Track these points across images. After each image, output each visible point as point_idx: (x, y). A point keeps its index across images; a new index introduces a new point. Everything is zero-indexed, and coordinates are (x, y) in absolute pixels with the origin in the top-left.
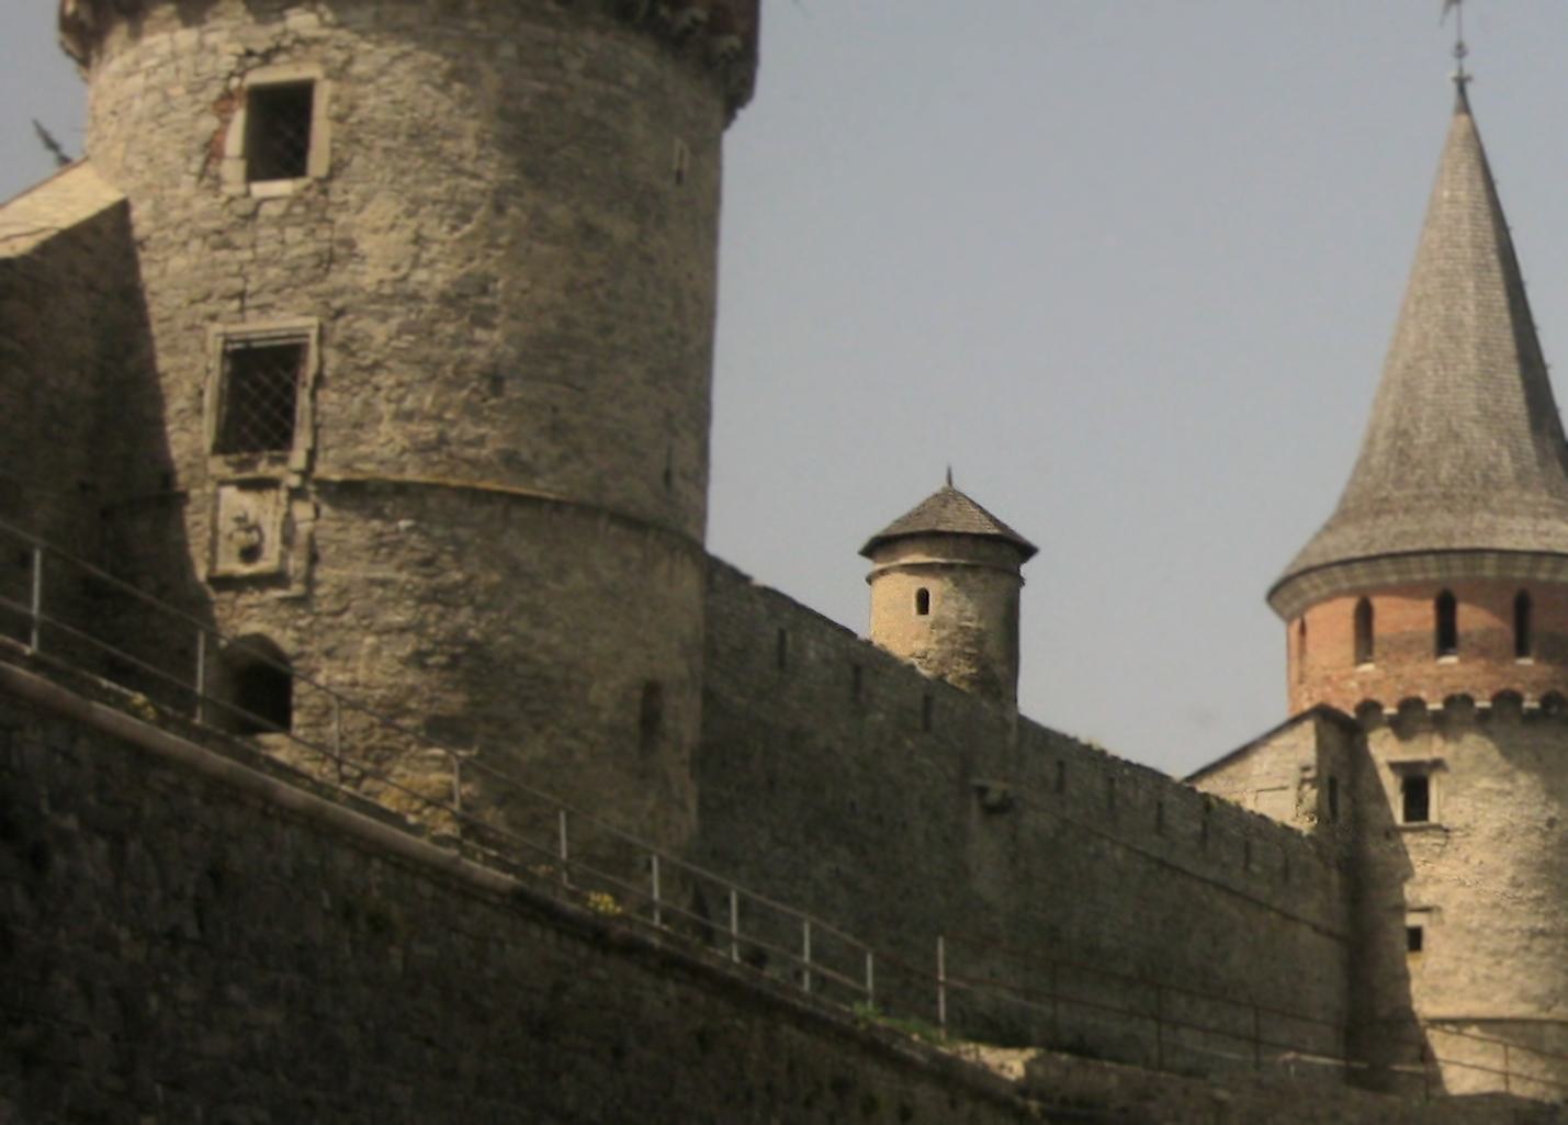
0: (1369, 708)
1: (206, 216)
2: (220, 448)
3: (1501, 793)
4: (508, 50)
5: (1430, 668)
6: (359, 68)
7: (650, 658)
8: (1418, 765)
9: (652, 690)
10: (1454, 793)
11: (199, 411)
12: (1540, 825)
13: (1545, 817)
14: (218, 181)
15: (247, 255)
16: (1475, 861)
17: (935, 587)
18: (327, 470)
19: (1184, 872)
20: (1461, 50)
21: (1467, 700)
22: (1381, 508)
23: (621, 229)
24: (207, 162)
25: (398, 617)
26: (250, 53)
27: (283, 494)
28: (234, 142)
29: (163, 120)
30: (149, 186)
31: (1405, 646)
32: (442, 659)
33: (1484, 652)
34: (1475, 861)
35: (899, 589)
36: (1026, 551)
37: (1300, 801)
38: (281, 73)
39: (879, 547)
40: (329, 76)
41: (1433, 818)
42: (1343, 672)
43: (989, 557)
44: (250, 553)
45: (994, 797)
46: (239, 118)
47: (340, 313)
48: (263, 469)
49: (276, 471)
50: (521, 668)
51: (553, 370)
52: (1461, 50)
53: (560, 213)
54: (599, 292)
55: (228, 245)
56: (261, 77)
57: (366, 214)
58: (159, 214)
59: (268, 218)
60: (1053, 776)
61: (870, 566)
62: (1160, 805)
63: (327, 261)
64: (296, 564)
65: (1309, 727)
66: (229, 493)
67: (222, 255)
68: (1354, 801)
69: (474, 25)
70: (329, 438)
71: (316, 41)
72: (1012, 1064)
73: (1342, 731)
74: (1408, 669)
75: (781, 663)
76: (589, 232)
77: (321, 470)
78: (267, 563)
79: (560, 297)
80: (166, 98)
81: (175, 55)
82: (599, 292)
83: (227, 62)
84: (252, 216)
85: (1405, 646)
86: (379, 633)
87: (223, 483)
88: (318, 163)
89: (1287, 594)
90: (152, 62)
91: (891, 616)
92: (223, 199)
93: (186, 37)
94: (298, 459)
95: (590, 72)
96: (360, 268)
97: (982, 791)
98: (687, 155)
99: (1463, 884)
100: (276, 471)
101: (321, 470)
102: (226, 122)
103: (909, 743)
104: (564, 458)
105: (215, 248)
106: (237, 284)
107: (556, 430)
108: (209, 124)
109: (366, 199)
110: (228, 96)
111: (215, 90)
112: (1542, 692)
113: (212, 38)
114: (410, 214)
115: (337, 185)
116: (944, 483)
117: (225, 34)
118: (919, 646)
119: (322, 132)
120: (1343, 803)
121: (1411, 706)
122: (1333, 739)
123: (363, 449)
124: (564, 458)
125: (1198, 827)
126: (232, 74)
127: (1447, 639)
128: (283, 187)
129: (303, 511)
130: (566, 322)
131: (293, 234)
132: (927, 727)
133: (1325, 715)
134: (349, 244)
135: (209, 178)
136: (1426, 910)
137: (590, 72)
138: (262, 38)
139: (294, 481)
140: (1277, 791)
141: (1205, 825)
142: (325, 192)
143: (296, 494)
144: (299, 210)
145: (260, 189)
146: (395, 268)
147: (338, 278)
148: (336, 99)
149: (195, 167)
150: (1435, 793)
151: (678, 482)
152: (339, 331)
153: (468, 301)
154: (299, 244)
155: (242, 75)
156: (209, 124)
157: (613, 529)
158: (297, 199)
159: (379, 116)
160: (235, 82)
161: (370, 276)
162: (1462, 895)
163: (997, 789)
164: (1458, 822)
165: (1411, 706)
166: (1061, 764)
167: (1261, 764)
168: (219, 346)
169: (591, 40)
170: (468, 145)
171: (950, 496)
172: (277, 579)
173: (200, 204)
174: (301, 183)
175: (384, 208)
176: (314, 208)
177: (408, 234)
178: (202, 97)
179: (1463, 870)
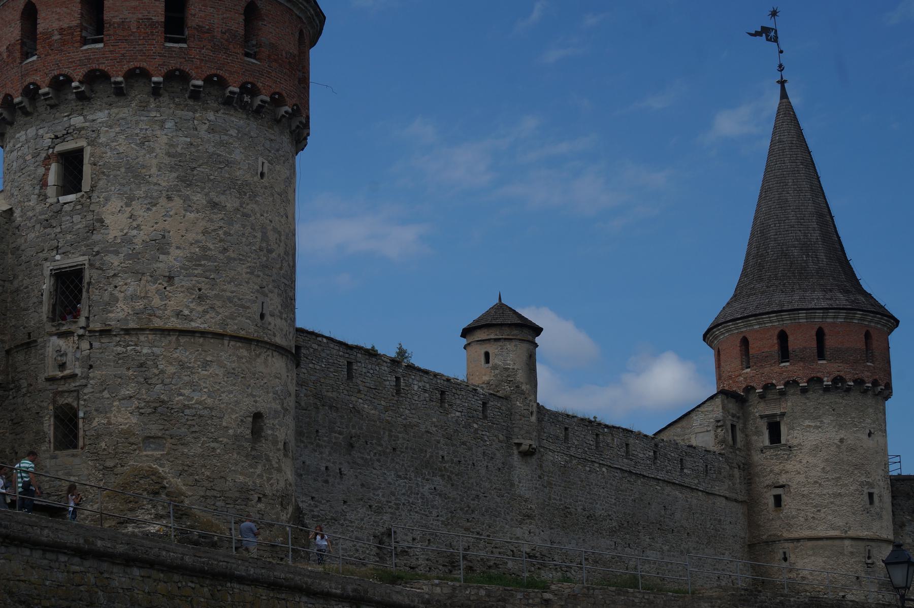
0: (749, 389)
1: (41, 214)
3: (817, 427)
4: (169, 124)
5: (776, 369)
6: (103, 139)
7: (256, 402)
8: (774, 415)
9: (258, 416)
10: (793, 429)
11: (41, 302)
12: (836, 441)
13: (838, 438)
14: (46, 197)
15: (58, 230)
16: (804, 461)
17: (492, 349)
18: (96, 326)
19: (644, 476)
20: (781, 68)
23: (230, 202)
24: (41, 188)
26: (56, 137)
27: (76, 338)
28: (52, 178)
29: (24, 171)
30: (20, 202)
32: (150, 410)
34: (804, 461)
36: (538, 330)
37: (716, 437)
38: (70, 145)
40: (89, 144)
41: (783, 442)
42: (737, 373)
44: (62, 366)
45: (525, 447)
46: (54, 167)
47: (98, 253)
49: (73, 328)
50: (187, 412)
51: (199, 271)
52: (781, 68)
53: (199, 198)
54: (221, 232)
55: (51, 226)
56: (59, 148)
57: (107, 206)
58: (23, 214)
59: (66, 212)
60: (562, 436)
61: (464, 341)
62: (627, 445)
63: (92, 230)
65: (718, 401)
66: (54, 338)
67: (48, 230)
68: (747, 435)
69: (153, 114)
71: (83, 128)
74: (767, 370)
75: (398, 392)
76: (214, 205)
77: (92, 326)
79: (200, 237)
80: (25, 161)
81: (27, 141)
82: (221, 232)
83: (47, 142)
84: (59, 212)
86: (120, 400)
87: (51, 335)
88: (86, 186)
90: (19, 145)
92: (48, 205)
94: (82, 321)
95: (211, 130)
96: (106, 231)
97: (519, 445)
98: (266, 164)
99: (799, 473)
100: (73, 328)
101: (92, 326)
102: (48, 169)
103: (475, 426)
104: (205, 312)
105: (45, 228)
106: (55, 243)
107: (201, 298)
108: (41, 171)
109: (107, 199)
110: (48, 157)
111: (43, 155)
112: (832, 377)
113: (41, 132)
114: (127, 205)
115: (95, 195)
116: (497, 301)
117: (46, 129)
118: (486, 378)
119: (87, 169)
120: (740, 436)
121: (768, 387)
122: (732, 406)
123: (111, 315)
124: (205, 312)
125: (652, 454)
126: (49, 147)
128: (71, 197)
129: (85, 345)
130: (204, 249)
131: (77, 218)
132: (485, 417)
134: (101, 221)
135: (43, 197)
136: (783, 486)
137: (211, 130)
138: (60, 130)
139: (81, 332)
141: (655, 452)
142: (90, 198)
144: (79, 207)
145: (63, 199)
146: (122, 230)
147: (96, 237)
148: (92, 155)
149: (37, 191)
150: (784, 429)
151: (268, 318)
154: (79, 222)
155: (53, 148)
156: (41, 171)
157: (232, 343)
158: (78, 202)
159: (112, 161)
160: (51, 151)
162: (801, 478)
163: (526, 444)
164: (795, 442)
165: (768, 387)
166: (566, 429)
167: (697, 420)
168: (49, 272)
169: (211, 116)
171: (501, 307)
173: (39, 208)
174: (79, 194)
176: (84, 207)
177: (127, 215)
178: (38, 159)
179: (798, 466)
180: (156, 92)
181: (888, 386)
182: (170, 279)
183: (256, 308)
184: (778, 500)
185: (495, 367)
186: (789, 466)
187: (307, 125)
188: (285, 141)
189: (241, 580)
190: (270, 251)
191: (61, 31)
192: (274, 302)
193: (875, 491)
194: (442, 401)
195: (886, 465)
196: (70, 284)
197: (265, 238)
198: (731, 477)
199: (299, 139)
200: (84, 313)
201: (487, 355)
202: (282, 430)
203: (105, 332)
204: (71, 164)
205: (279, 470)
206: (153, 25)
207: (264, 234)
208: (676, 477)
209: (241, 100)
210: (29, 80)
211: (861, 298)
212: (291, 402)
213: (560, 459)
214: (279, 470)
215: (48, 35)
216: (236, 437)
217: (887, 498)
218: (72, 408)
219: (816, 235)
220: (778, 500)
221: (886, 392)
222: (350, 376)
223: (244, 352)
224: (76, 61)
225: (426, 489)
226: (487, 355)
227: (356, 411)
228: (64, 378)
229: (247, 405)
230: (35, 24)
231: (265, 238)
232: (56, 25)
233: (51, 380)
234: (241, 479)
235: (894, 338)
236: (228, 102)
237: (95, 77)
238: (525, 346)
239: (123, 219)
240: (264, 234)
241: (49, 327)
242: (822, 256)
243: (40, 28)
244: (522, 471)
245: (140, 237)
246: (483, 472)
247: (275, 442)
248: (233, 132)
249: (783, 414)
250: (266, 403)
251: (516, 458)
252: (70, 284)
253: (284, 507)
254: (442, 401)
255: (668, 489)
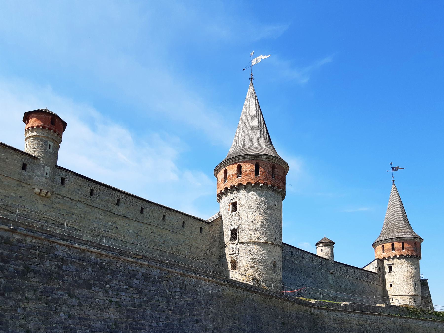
0: (384, 258)
2: (230, 240)
5: (391, 253)
8: (390, 264)
9: (275, 262)
17: (323, 248)
21: (403, 255)
22: (384, 234)
25: (246, 257)
28: (231, 209)
31: (388, 250)
33: (398, 250)
35: (319, 249)
36: (334, 243)
39: (317, 244)
43: (331, 244)
45: (331, 272)
46: (231, 206)
48: (234, 242)
49: (235, 242)
56: (232, 202)
64: (237, 252)
70: (240, 238)
72: (314, 302)
73: (381, 261)
74: (388, 253)
75: (302, 258)
78: (234, 252)
83: (230, 201)
85: (388, 250)
88: (238, 210)
89: (374, 245)
91: (322, 252)
93: (226, 198)
100: (235, 242)
119: (238, 206)
122: (380, 262)
127: (393, 249)
129: (238, 246)
133: (378, 259)
135: (228, 213)
140: (373, 268)
143: (237, 244)
151: (277, 239)
152: (240, 227)
153: (253, 222)
154: (237, 218)
156: (228, 207)
161: (243, 220)
162: (397, 280)
169: (265, 192)
170: (252, 205)
172: (235, 253)
175: (244, 213)
180: (253, 187)
181: (420, 257)
182: (256, 230)
183: (274, 237)
184: (391, 286)
185: (324, 253)
186: (394, 277)
187: (285, 194)
188: (281, 197)
189: (276, 298)
190: (277, 223)
191: (233, 175)
192: (278, 235)
193: (416, 283)
194: (312, 260)
195: (419, 277)
196: (234, 233)
197: (276, 220)
198: (379, 280)
199: (283, 197)
200: (237, 239)
201: (322, 250)
202: (280, 265)
203: (242, 243)
204: (234, 205)
205: (279, 274)
206: (252, 171)
207: (276, 219)
208: (366, 280)
209: (271, 188)
210: (226, 187)
211: (414, 234)
212: (282, 259)
213: (339, 275)
214: (279, 274)
215: (230, 176)
216: (270, 267)
217: (420, 285)
218: (235, 260)
219: (402, 219)
220: (391, 286)
221: (420, 258)
222: (292, 255)
223: (272, 247)
224: (235, 182)
225: (308, 281)
226: (322, 250)
227: (293, 262)
228: (234, 254)
229: (273, 259)
230: (227, 174)
231: (276, 220)
232: (231, 174)
233: (230, 254)
234: (271, 276)
235: (422, 244)
236: (268, 188)
237: (240, 185)
238: (331, 247)
239: (246, 217)
240: (276, 219)
241: (230, 242)
242: (403, 224)
243: (228, 175)
244: (330, 277)
245: (249, 221)
246: (321, 277)
247: (278, 268)
248: (269, 196)
249: (393, 264)
250: (276, 259)
251: (329, 275)
252: (234, 233)
253: (280, 284)
254: (312, 260)
255: (364, 282)
